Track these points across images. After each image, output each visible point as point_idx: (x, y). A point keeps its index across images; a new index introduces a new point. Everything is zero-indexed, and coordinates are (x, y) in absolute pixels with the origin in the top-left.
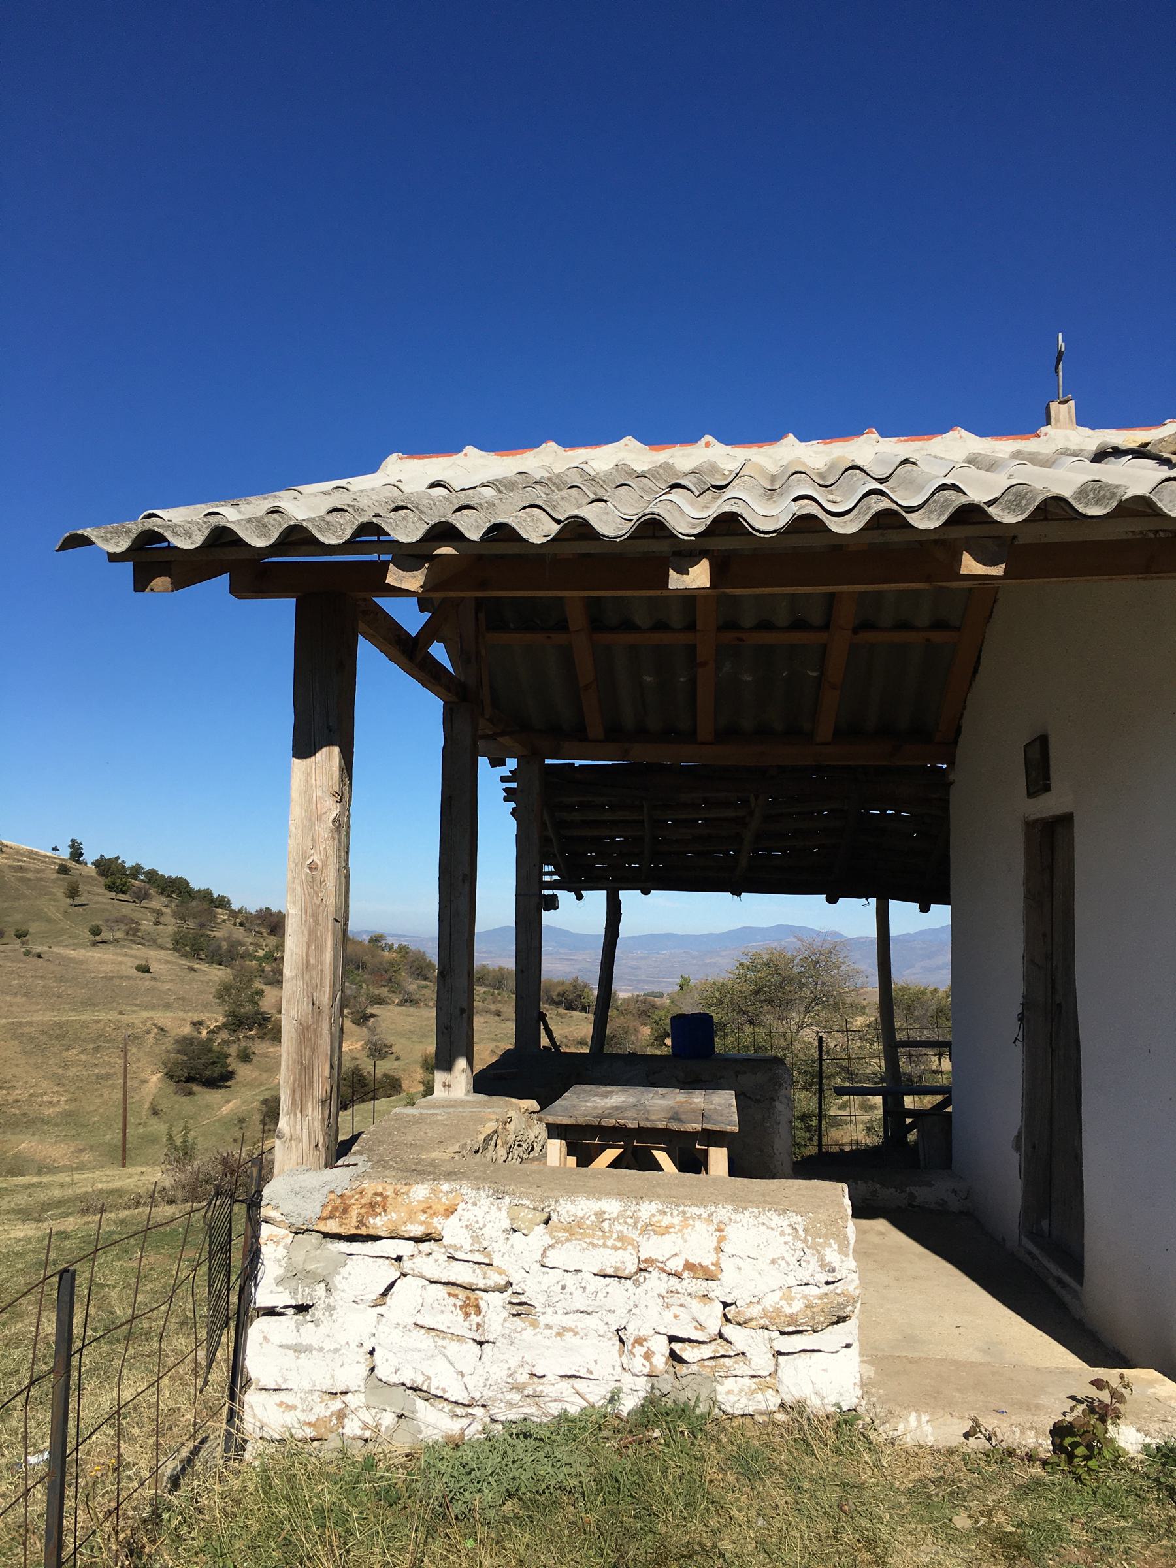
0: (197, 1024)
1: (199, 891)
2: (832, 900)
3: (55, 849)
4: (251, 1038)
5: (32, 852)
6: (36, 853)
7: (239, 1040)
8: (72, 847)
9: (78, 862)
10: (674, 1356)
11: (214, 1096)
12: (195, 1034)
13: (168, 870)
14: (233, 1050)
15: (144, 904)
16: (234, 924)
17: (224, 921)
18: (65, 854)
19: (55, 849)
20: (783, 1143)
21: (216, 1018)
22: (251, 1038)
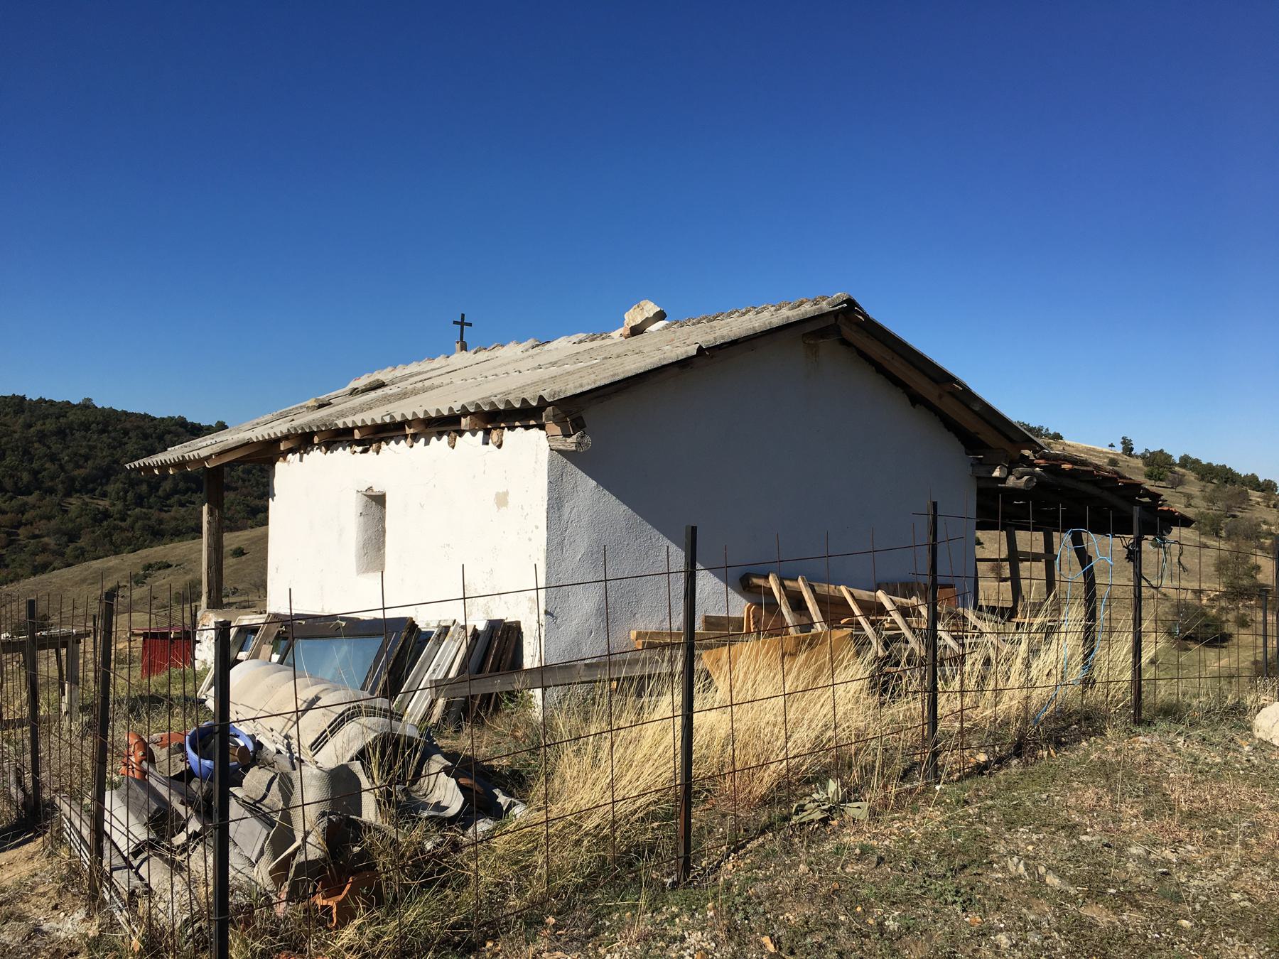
0: (1198, 592)
1: (1246, 476)
2: (1161, 451)
3: (1111, 446)
4: (1251, 607)
5: (1090, 449)
6: (1094, 450)
7: (1238, 608)
8: (1124, 443)
9: (1130, 455)
10: (631, 679)
11: (1211, 654)
12: (1196, 602)
13: (1209, 455)
14: (1231, 616)
15: (1179, 489)
16: (1268, 506)
17: (1258, 503)
18: (1119, 449)
19: (1111, 446)
20: (192, 523)
21: (1214, 586)
22: (1251, 607)
